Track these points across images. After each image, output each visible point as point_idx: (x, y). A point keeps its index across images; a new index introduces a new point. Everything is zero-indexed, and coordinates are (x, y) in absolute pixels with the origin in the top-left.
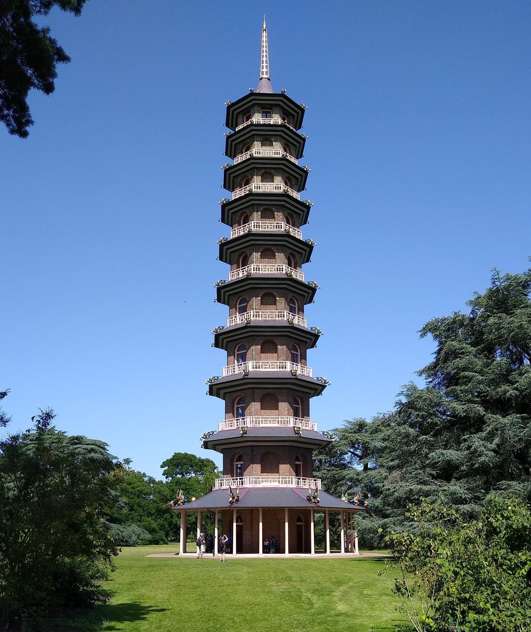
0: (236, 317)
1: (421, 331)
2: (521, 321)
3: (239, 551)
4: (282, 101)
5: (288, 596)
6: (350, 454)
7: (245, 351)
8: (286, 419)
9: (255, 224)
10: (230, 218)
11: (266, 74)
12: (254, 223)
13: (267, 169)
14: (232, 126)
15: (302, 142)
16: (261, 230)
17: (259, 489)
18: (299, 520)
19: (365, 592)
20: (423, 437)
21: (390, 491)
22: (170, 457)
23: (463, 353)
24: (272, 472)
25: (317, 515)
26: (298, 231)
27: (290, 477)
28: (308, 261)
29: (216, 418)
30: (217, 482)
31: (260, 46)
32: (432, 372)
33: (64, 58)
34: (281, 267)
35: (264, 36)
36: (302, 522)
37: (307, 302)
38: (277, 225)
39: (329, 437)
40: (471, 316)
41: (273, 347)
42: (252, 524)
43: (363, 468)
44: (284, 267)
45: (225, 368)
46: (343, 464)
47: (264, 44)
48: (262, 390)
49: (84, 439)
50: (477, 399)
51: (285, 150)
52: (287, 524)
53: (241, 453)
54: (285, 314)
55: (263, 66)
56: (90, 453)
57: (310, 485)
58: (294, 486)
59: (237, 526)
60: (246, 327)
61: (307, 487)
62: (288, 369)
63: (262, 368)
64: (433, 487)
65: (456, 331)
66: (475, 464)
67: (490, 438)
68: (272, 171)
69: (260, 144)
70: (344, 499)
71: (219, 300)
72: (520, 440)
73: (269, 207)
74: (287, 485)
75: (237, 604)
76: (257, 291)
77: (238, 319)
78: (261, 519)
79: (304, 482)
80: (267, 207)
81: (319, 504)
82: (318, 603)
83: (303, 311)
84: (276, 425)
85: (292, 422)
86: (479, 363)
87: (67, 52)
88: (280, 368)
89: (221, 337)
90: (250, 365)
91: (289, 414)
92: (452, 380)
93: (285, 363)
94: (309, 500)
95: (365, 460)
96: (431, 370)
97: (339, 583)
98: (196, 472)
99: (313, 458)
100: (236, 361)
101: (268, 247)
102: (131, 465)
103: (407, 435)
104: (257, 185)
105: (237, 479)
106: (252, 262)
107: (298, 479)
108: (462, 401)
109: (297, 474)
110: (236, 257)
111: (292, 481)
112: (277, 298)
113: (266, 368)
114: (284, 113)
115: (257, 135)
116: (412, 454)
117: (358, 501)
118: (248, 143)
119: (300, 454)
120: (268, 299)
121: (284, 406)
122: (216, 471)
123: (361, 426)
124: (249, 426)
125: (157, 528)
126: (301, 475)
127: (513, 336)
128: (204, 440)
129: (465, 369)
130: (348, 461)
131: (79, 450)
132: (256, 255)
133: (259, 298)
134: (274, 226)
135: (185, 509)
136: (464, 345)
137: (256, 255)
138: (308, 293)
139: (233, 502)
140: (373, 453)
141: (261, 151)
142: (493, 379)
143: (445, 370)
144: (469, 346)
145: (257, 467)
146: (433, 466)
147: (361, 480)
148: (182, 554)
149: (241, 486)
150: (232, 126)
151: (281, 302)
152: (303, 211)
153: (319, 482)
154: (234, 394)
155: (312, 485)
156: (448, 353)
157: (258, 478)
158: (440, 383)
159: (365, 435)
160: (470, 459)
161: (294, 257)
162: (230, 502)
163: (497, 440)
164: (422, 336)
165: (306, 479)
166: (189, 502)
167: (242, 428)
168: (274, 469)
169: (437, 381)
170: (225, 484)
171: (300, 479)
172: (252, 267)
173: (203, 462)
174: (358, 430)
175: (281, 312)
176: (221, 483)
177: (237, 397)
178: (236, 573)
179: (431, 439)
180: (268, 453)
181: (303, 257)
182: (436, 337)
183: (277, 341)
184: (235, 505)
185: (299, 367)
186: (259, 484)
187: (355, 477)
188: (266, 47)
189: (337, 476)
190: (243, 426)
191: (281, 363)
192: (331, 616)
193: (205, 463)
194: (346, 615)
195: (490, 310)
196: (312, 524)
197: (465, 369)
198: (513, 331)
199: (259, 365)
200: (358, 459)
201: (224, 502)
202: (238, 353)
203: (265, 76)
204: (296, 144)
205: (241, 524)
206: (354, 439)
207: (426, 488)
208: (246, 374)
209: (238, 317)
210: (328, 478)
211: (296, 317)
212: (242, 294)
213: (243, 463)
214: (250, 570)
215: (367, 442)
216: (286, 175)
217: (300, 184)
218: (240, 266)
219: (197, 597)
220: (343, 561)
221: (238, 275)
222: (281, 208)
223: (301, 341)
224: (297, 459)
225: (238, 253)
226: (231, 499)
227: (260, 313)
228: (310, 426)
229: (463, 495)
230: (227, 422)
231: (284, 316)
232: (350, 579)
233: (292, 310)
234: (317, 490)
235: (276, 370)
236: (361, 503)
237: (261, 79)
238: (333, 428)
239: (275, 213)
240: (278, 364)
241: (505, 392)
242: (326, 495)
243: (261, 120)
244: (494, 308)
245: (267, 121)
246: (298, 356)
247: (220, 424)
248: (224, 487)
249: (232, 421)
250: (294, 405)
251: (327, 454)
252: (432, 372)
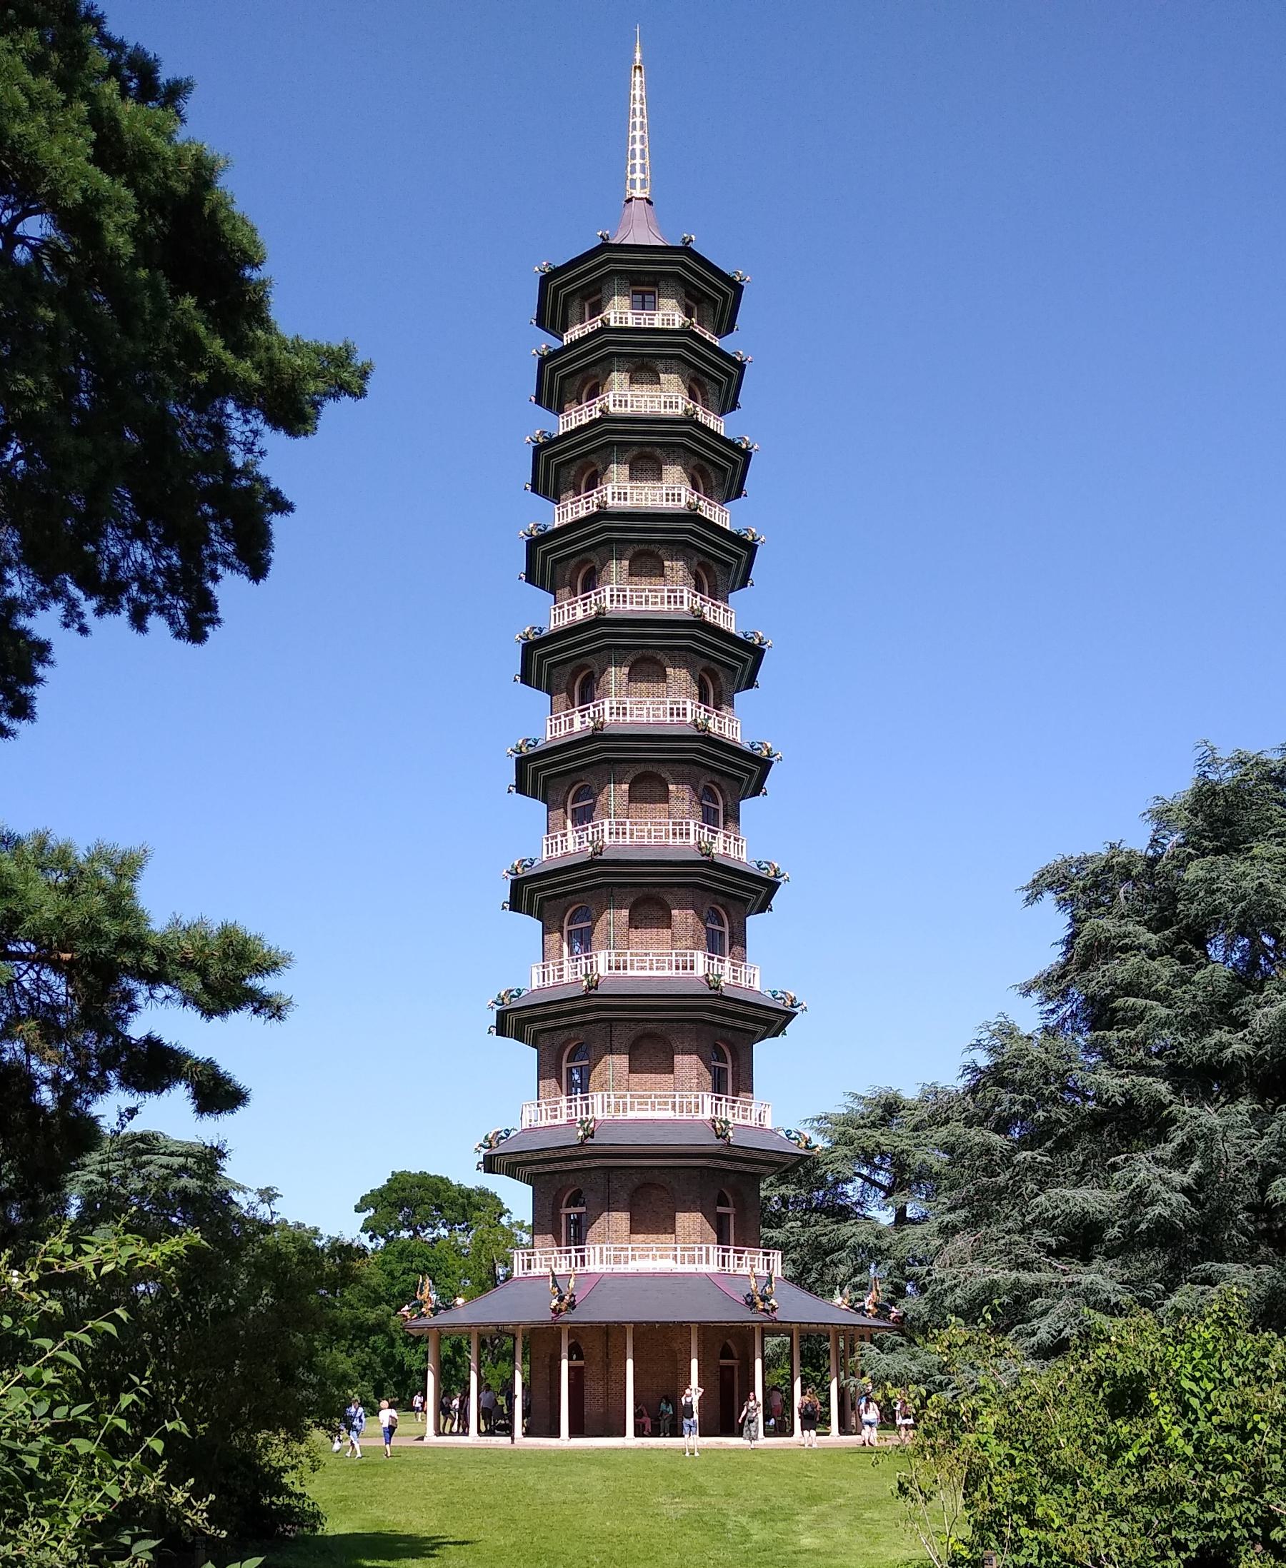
0: (565, 835)
1: (1027, 888)
2: (1259, 878)
3: (575, 1431)
4: (685, 346)
5: (697, 1521)
6: (859, 1181)
7: (589, 924)
8: (693, 1100)
9: (615, 593)
10: (548, 574)
11: (643, 187)
12: (612, 590)
13: (646, 445)
14: (553, 327)
15: (735, 372)
16: (630, 608)
17: (625, 1275)
18: (726, 1353)
19: (867, 1515)
20: (1025, 1153)
21: (946, 1286)
22: (380, 1182)
23: (1125, 949)
24: (657, 1232)
25: (772, 1342)
26: (726, 611)
27: (700, 1093)
28: (751, 684)
29: (512, 1095)
30: (518, 1259)
31: (626, 112)
32: (1055, 988)
33: (283, 506)
34: (678, 594)
35: (638, 83)
36: (733, 1358)
37: (749, 793)
38: (667, 596)
39: (803, 1144)
40: (1150, 853)
41: (661, 913)
42: (608, 1365)
43: (893, 1219)
44: (688, 706)
45: (531, 963)
46: (843, 1208)
47: (638, 106)
49: (161, 1139)
50: (1158, 1062)
51: (692, 396)
52: (694, 1363)
53: (576, 1184)
54: (692, 828)
55: (633, 165)
56: (179, 1177)
57: (753, 1267)
58: (713, 1267)
59: (570, 1368)
60: (590, 863)
61: (745, 1270)
62: (700, 971)
63: (632, 969)
64: (1046, 1277)
65: (1112, 888)
66: (1140, 1222)
67: (1184, 1154)
68: (658, 451)
69: (627, 381)
70: (838, 1300)
71: (521, 788)
72: (1252, 1164)
73: (652, 547)
74: (697, 1265)
75: (589, 1534)
76: (618, 768)
77: (571, 841)
78: (630, 1351)
79: (739, 1259)
80: (642, 547)
81: (775, 1314)
82: (759, 1533)
83: (737, 820)
84: (669, 1114)
85: (706, 1107)
86: (1165, 970)
87: (289, 495)
88: (677, 968)
89: (528, 887)
90: (602, 961)
91: (700, 1087)
92: (1100, 1014)
93: (692, 955)
94: (752, 1304)
95: (899, 1198)
96: (1053, 984)
97: (814, 1499)
98: (450, 1224)
99: (762, 1194)
100: (565, 945)
101: (650, 653)
102: (278, 1205)
103: (988, 1150)
104: (622, 491)
105: (569, 1251)
106: (607, 694)
107: (724, 1250)
108: (1120, 1067)
109: (722, 1240)
110: (566, 678)
111: (708, 1255)
112: (671, 787)
113: (642, 968)
114: (688, 295)
115: (619, 355)
116: (1000, 1192)
117: (875, 1305)
118: (595, 376)
119: (726, 1187)
120: (648, 788)
121: (688, 1064)
122: (504, 1220)
123: (890, 1109)
124: (599, 1116)
125: (354, 1374)
126: (732, 1241)
127: (1244, 911)
128: (484, 1151)
129: (1130, 989)
130: (854, 1200)
131: (151, 1168)
132: (616, 675)
133: (626, 787)
134: (663, 597)
135: (438, 1327)
136: (1131, 928)
137: (616, 675)
138: (751, 772)
139: (560, 1311)
140: (919, 1177)
141: (629, 399)
142: (1194, 1015)
143: (1087, 988)
144: (1142, 929)
145: (621, 1220)
146: (1046, 1223)
147: (888, 1250)
148: (431, 1438)
149: (579, 1270)
150: (553, 327)
151: (680, 794)
152: (739, 557)
153: (777, 1256)
154: (563, 1034)
155: (758, 1267)
156: (1092, 945)
157: (622, 1249)
158: (1076, 1015)
159: (899, 1132)
160: (1132, 1210)
161: (714, 677)
162: (554, 1310)
163: (1196, 1166)
164: (1029, 901)
165: (743, 1252)
166: (448, 1308)
167: (582, 1122)
168: (665, 1225)
169: (1066, 1009)
170: (541, 1263)
171: (728, 1251)
172: (607, 706)
173: (469, 1197)
174: (882, 1118)
175: (681, 824)
176: (529, 1261)
177: (568, 1041)
178: (577, 1478)
179: (1045, 1159)
180: (649, 1184)
181: (738, 677)
182: (1063, 904)
183: (669, 899)
184: (565, 1317)
185: (727, 965)
186: (626, 1262)
187: (872, 1241)
188: (642, 128)
189: (824, 1240)
190: (584, 1116)
191: (681, 955)
192: (785, 1553)
193: (476, 1199)
194: (816, 1552)
195: (1196, 846)
196: (758, 1363)
197: (1130, 989)
198: (1243, 898)
199: (625, 962)
200: (882, 1194)
201: (539, 1310)
202: (572, 927)
203: (638, 193)
204: (718, 379)
205: (581, 1363)
206: (870, 1145)
207: (1028, 1278)
208: (593, 986)
209: (569, 834)
210: (801, 1246)
211: (720, 836)
212: (582, 775)
213: (583, 1209)
214: (607, 1473)
215: (903, 1152)
216: (695, 461)
217: (732, 483)
218: (576, 703)
219: (501, 1523)
220: (830, 1454)
221: (571, 725)
222: (681, 549)
223: (731, 898)
224: (722, 1201)
225: (569, 668)
226: (555, 1302)
227: (628, 827)
228: (755, 1115)
229: (1112, 1296)
230: (544, 1107)
231: (688, 834)
232: (842, 1492)
233: (709, 817)
234: (769, 1280)
235: (667, 973)
236: (882, 1311)
237: (630, 200)
238: (817, 1114)
239: (667, 563)
240: (674, 958)
241: (1222, 1047)
242: (793, 1291)
243: (630, 316)
244: (1204, 837)
246: (726, 937)
247: (526, 1110)
248: (536, 1271)
249: (557, 1102)
250: (714, 1063)
251: (799, 1183)
252: (1055, 988)
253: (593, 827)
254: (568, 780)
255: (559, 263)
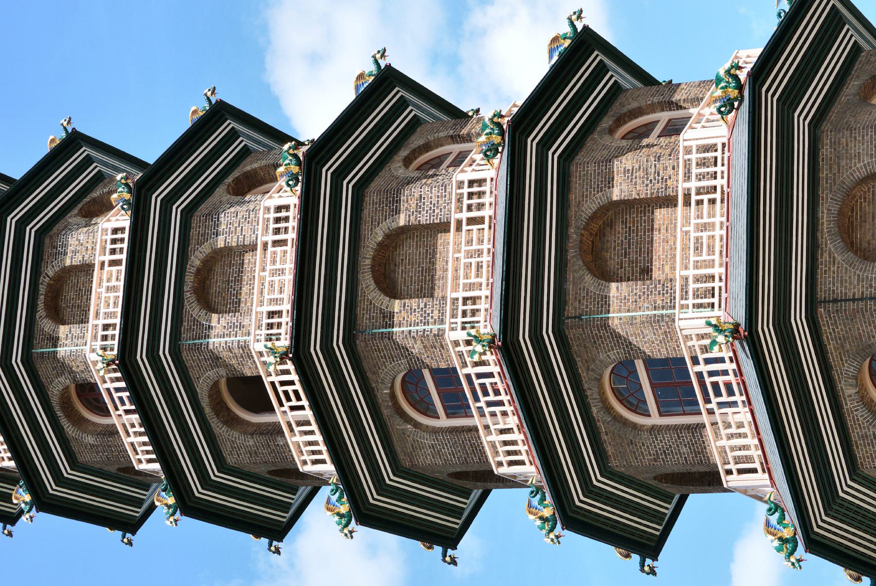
7: (640, 366)
16: (487, 289)
38: (463, 210)
48: (823, 258)
73: (42, 289)
76: (364, 318)
93: (688, 151)
112: (402, 222)
183: (586, 205)
225: (219, 428)
239: (68, 263)
245: (106, 295)
253: (464, 365)
254: (396, 425)
255: (608, 552)
